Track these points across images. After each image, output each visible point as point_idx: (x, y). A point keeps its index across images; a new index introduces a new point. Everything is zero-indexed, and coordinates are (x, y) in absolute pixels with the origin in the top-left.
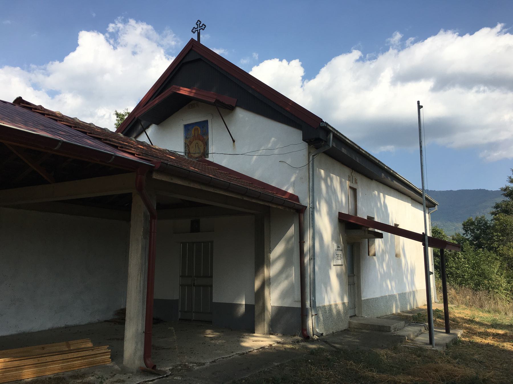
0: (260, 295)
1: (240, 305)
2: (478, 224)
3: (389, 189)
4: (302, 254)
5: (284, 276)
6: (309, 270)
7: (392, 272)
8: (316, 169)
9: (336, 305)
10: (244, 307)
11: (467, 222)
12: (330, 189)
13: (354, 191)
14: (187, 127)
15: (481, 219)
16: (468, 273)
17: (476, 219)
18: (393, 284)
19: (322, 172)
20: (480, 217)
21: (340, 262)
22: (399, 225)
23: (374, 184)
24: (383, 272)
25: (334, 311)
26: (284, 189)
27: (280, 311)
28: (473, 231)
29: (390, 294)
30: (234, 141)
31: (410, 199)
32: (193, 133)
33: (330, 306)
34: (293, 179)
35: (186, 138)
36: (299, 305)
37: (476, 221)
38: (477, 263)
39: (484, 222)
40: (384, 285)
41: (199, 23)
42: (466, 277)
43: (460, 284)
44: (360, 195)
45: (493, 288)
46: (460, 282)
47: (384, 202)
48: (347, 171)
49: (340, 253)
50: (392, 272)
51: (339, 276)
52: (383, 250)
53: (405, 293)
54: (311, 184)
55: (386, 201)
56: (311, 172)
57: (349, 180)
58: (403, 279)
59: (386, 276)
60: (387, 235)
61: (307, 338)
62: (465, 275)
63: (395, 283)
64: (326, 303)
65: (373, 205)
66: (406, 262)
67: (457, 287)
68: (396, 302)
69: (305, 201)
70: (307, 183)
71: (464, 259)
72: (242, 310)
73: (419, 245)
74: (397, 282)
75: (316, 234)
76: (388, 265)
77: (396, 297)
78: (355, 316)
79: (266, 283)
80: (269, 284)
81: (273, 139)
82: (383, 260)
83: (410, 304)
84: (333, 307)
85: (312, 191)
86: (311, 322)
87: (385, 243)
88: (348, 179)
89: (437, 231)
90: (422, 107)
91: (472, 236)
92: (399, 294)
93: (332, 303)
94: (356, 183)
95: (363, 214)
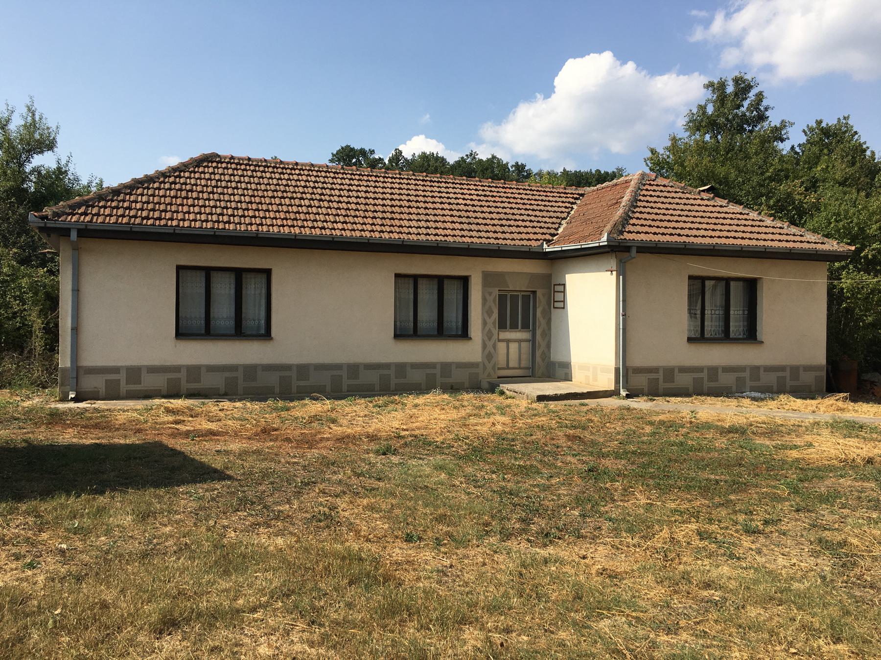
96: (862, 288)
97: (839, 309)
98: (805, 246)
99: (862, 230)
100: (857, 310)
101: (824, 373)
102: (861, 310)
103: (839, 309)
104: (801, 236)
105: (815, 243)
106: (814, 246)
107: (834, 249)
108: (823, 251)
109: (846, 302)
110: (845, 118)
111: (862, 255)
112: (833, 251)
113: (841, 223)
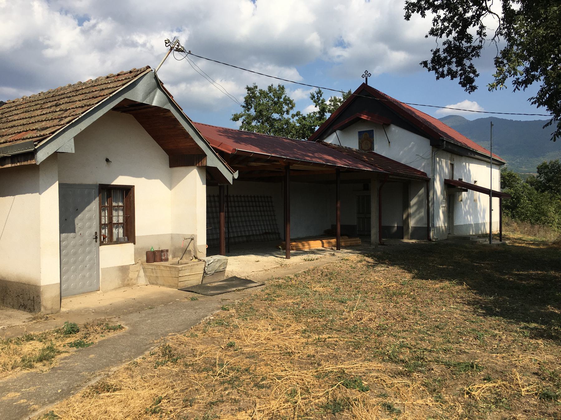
0: (406, 222)
1: (394, 227)
2: (551, 168)
3: (472, 159)
4: (428, 202)
5: (418, 212)
6: (431, 209)
7: (471, 210)
8: (435, 158)
9: (442, 227)
10: (396, 227)
11: (542, 166)
12: (441, 167)
13: (452, 165)
14: (360, 133)
15: (555, 162)
16: (530, 212)
17: (550, 162)
18: (472, 218)
19: (438, 159)
20: (554, 161)
21: (444, 205)
22: (452, 79)
23: (463, 158)
24: (465, 211)
25: (441, 230)
26: (418, 169)
27: (415, 229)
28: (546, 174)
29: (469, 223)
30: (389, 142)
31: (486, 162)
32: (364, 136)
33: (439, 227)
34: (423, 164)
35: (359, 139)
36: (426, 226)
37: (550, 165)
38: (539, 204)
39: (557, 166)
40: (466, 218)
41: (366, 72)
42: (528, 215)
43: (522, 220)
44: (455, 167)
45: (548, 223)
46: (523, 219)
47: (469, 168)
48: (449, 155)
49: (444, 200)
50: (471, 210)
51: (443, 212)
52: (466, 198)
53: (479, 224)
54: (433, 167)
55: (470, 168)
56: (433, 161)
57: (450, 160)
58: (478, 215)
59: (468, 213)
60: (470, 191)
61: (430, 240)
62: (527, 213)
63: (473, 217)
64: (438, 226)
65: (462, 171)
66: (481, 206)
67: (519, 222)
68: (473, 228)
69: (430, 176)
70: (431, 167)
71: (528, 200)
72: (395, 229)
73: (487, 196)
74: (474, 216)
75: (435, 192)
76: (469, 206)
77: (473, 226)
78: (450, 234)
79: (409, 216)
80: (410, 216)
81: (412, 143)
82: (466, 204)
83: (481, 231)
84: (441, 227)
85: (434, 170)
86: (431, 234)
87: (468, 194)
88: (449, 159)
89: (511, 175)
90: (493, 125)
91: (545, 178)
92: (474, 224)
93: (440, 226)
94: (454, 160)
95: (456, 178)
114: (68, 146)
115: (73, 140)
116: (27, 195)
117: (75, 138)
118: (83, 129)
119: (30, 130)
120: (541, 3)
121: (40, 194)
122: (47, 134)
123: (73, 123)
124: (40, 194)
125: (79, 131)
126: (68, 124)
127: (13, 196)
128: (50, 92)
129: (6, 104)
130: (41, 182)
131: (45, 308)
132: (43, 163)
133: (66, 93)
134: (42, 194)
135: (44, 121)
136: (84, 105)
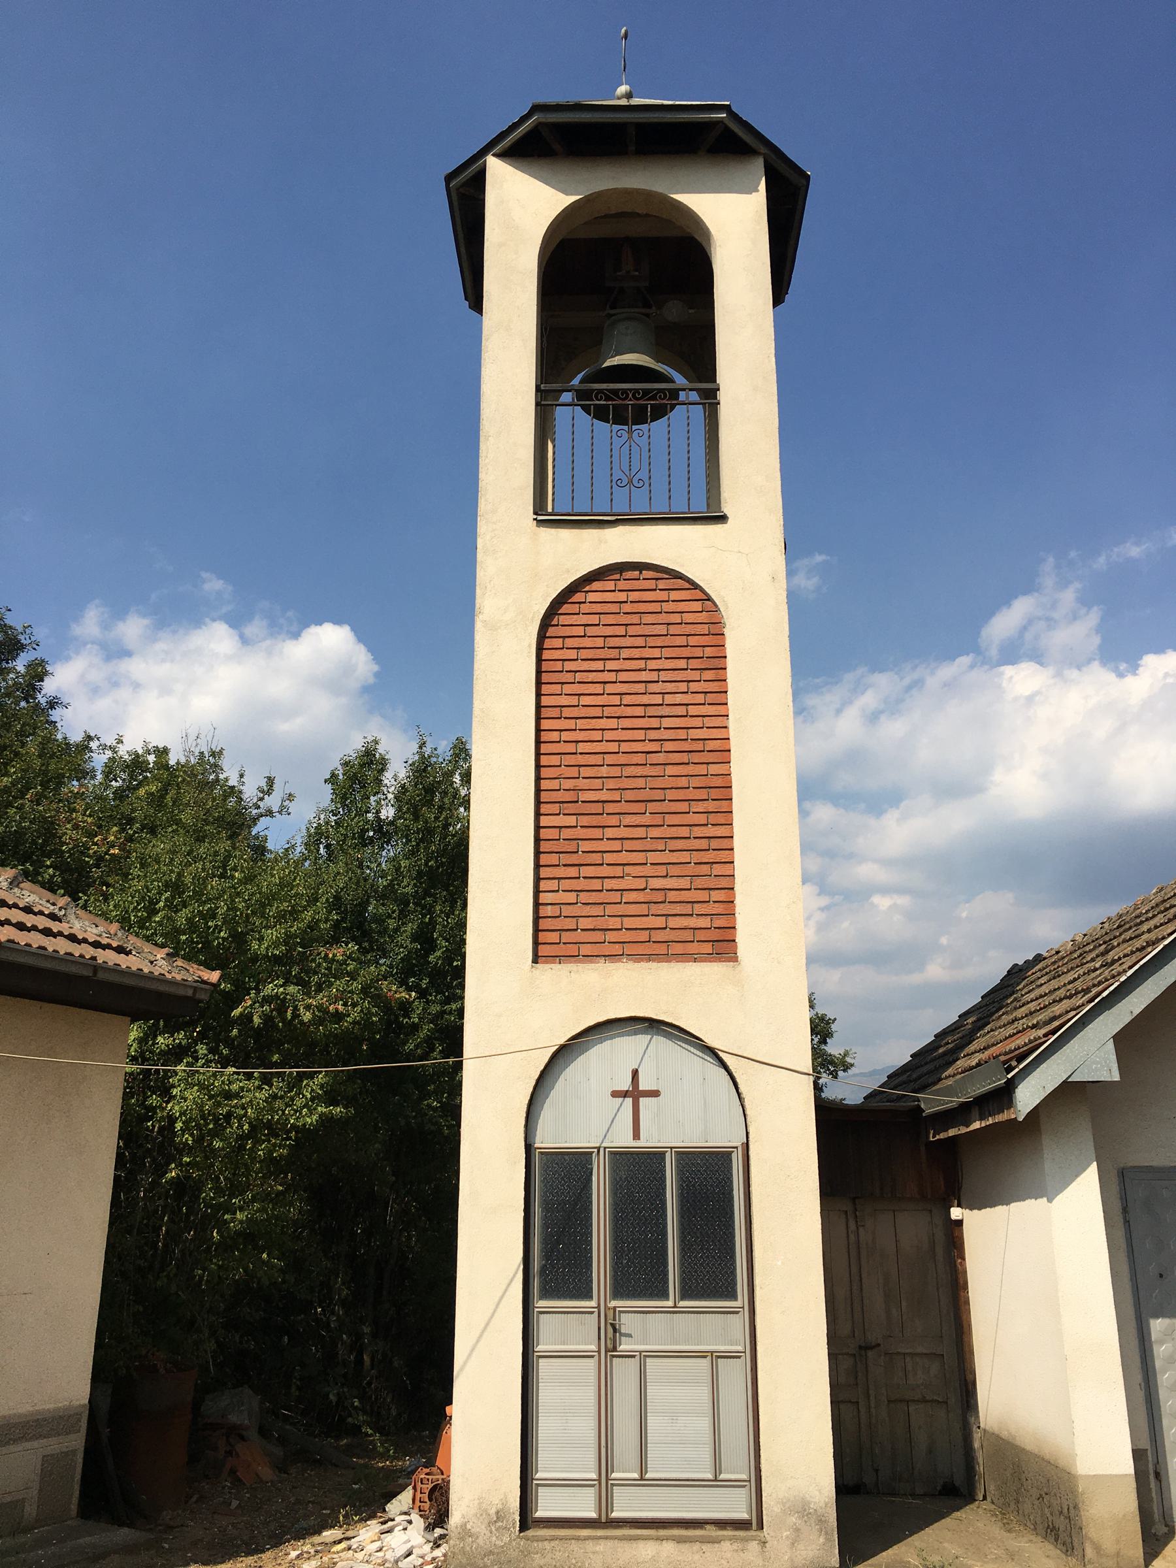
96: (228, 1116)
97: (155, 1184)
98: (62, 946)
99: (240, 939)
100: (208, 1193)
101: (76, 1442)
102: (218, 1190)
103: (155, 1184)
104: (53, 917)
105: (96, 945)
106: (89, 952)
107: (157, 971)
108: (116, 969)
109: (180, 1164)
110: (213, 754)
111: (236, 1012)
112: (150, 977)
113: (185, 913)
114: (1097, 1063)
115: (1111, 1045)
116: (1028, 1202)
117: (1118, 1038)
118: (1137, 1011)
119: (1028, 1027)
120: (149, 896)
121: (1050, 1201)
122: (1040, 1038)
123: (1103, 998)
124: (1050, 1201)
125: (1127, 1019)
126: (1093, 1004)
127: (1007, 1205)
128: (1121, 915)
129: (1045, 959)
130: (1049, 1166)
131: (1098, 1548)
132: (1034, 1113)
133: (1144, 911)
134: (1055, 1201)
135: (1064, 998)
136: (1145, 944)
